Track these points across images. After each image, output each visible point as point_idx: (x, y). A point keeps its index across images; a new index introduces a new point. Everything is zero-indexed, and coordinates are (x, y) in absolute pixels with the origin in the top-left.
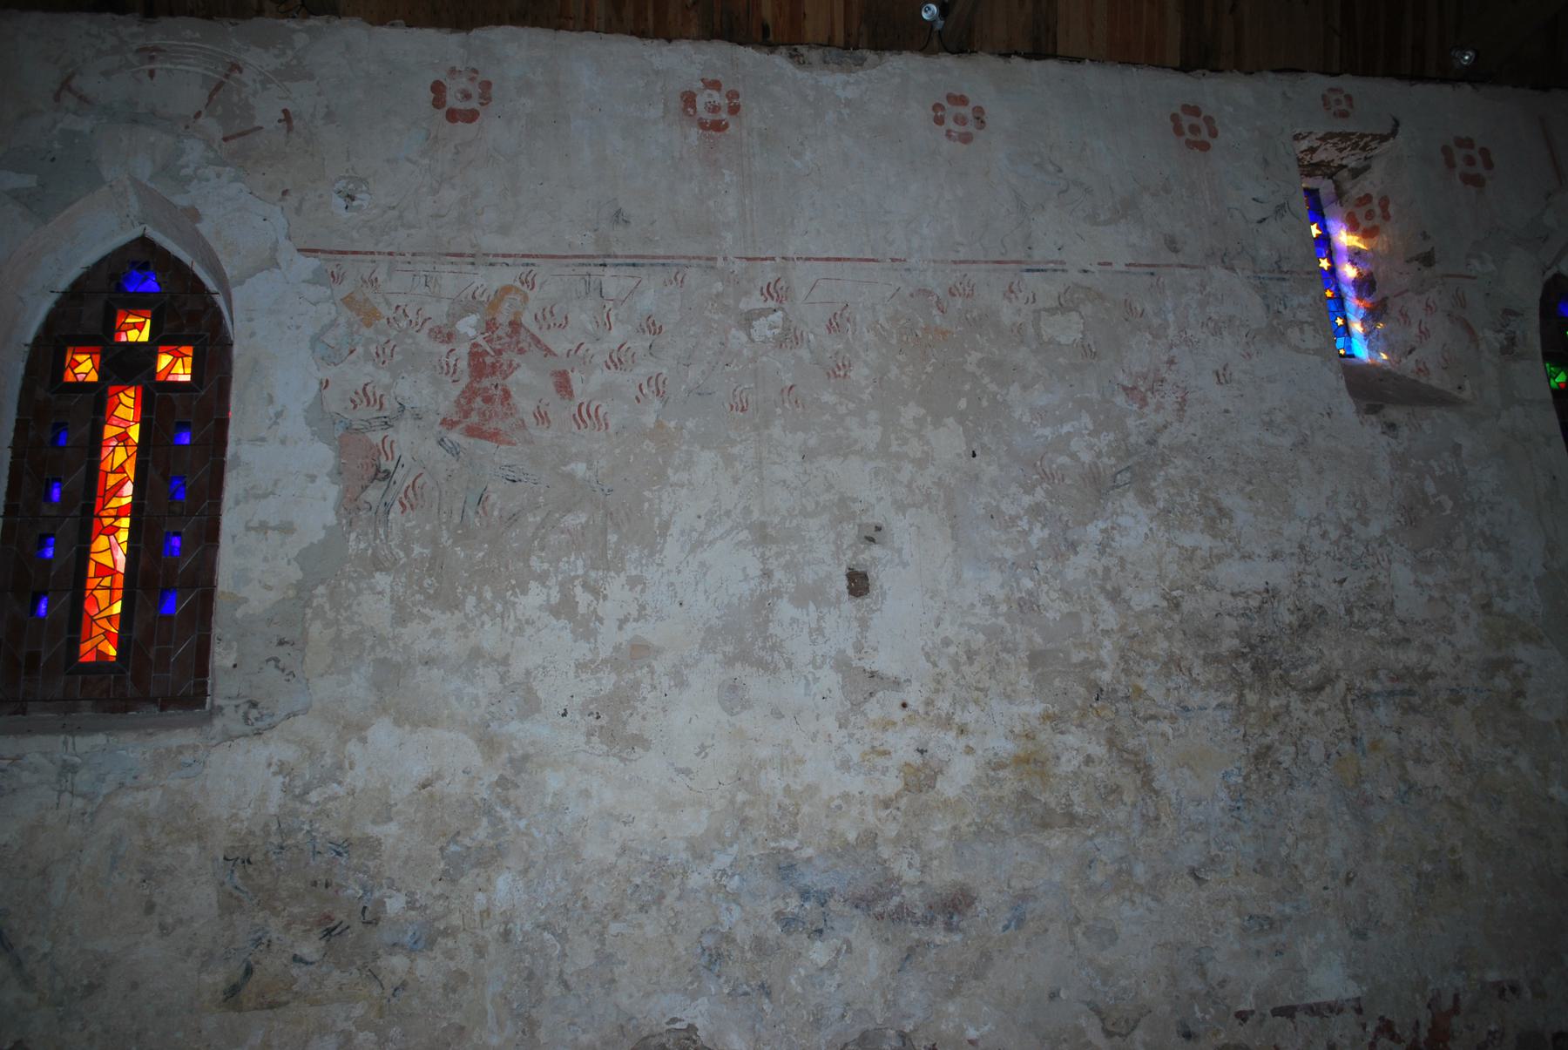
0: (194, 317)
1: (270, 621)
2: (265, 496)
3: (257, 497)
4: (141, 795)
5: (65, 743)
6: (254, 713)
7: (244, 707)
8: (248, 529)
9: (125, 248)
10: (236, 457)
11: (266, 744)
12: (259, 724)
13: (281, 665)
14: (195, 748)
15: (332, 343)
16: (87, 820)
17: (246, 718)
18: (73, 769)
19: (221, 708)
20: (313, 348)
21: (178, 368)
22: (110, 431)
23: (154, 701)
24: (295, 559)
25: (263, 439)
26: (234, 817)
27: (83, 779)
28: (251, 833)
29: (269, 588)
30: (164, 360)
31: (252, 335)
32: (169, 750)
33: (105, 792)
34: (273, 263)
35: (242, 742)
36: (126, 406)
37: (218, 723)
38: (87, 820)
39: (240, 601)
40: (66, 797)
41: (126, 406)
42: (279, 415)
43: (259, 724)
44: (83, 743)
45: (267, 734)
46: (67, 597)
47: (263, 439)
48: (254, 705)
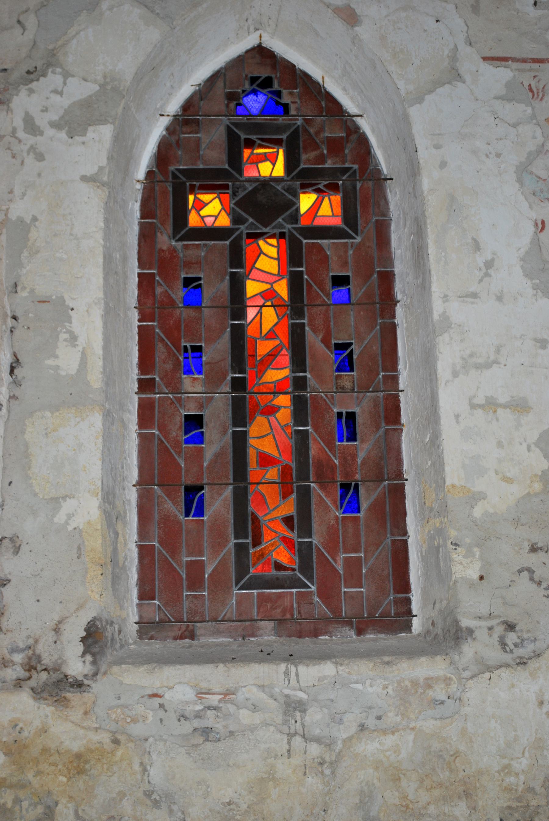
0: (333, 150)
1: (517, 522)
2: (488, 365)
3: (478, 367)
4: (390, 740)
5: (287, 674)
6: (512, 638)
7: (499, 630)
8: (473, 406)
9: (239, 62)
10: (445, 317)
11: (533, 675)
12: (520, 652)
13: (536, 577)
14: (447, 681)
15: (543, 174)
16: (327, 772)
17: (503, 644)
18: (300, 706)
19: (470, 631)
20: (520, 181)
21: (325, 209)
22: (252, 288)
23: (348, 622)
24: (537, 444)
25: (474, 295)
26: (507, 769)
27: (315, 717)
28: (530, 790)
29: (508, 480)
30: (306, 201)
31: (443, 165)
32: (415, 683)
33: (345, 736)
34: (454, 75)
35: (504, 673)
36: (268, 256)
37: (469, 650)
38: (327, 772)
39: (476, 498)
40: (298, 741)
41: (268, 256)
42: (489, 264)
43: (520, 652)
44: (310, 673)
45: (533, 665)
46: (228, 492)
47: (474, 295)
48: (511, 627)
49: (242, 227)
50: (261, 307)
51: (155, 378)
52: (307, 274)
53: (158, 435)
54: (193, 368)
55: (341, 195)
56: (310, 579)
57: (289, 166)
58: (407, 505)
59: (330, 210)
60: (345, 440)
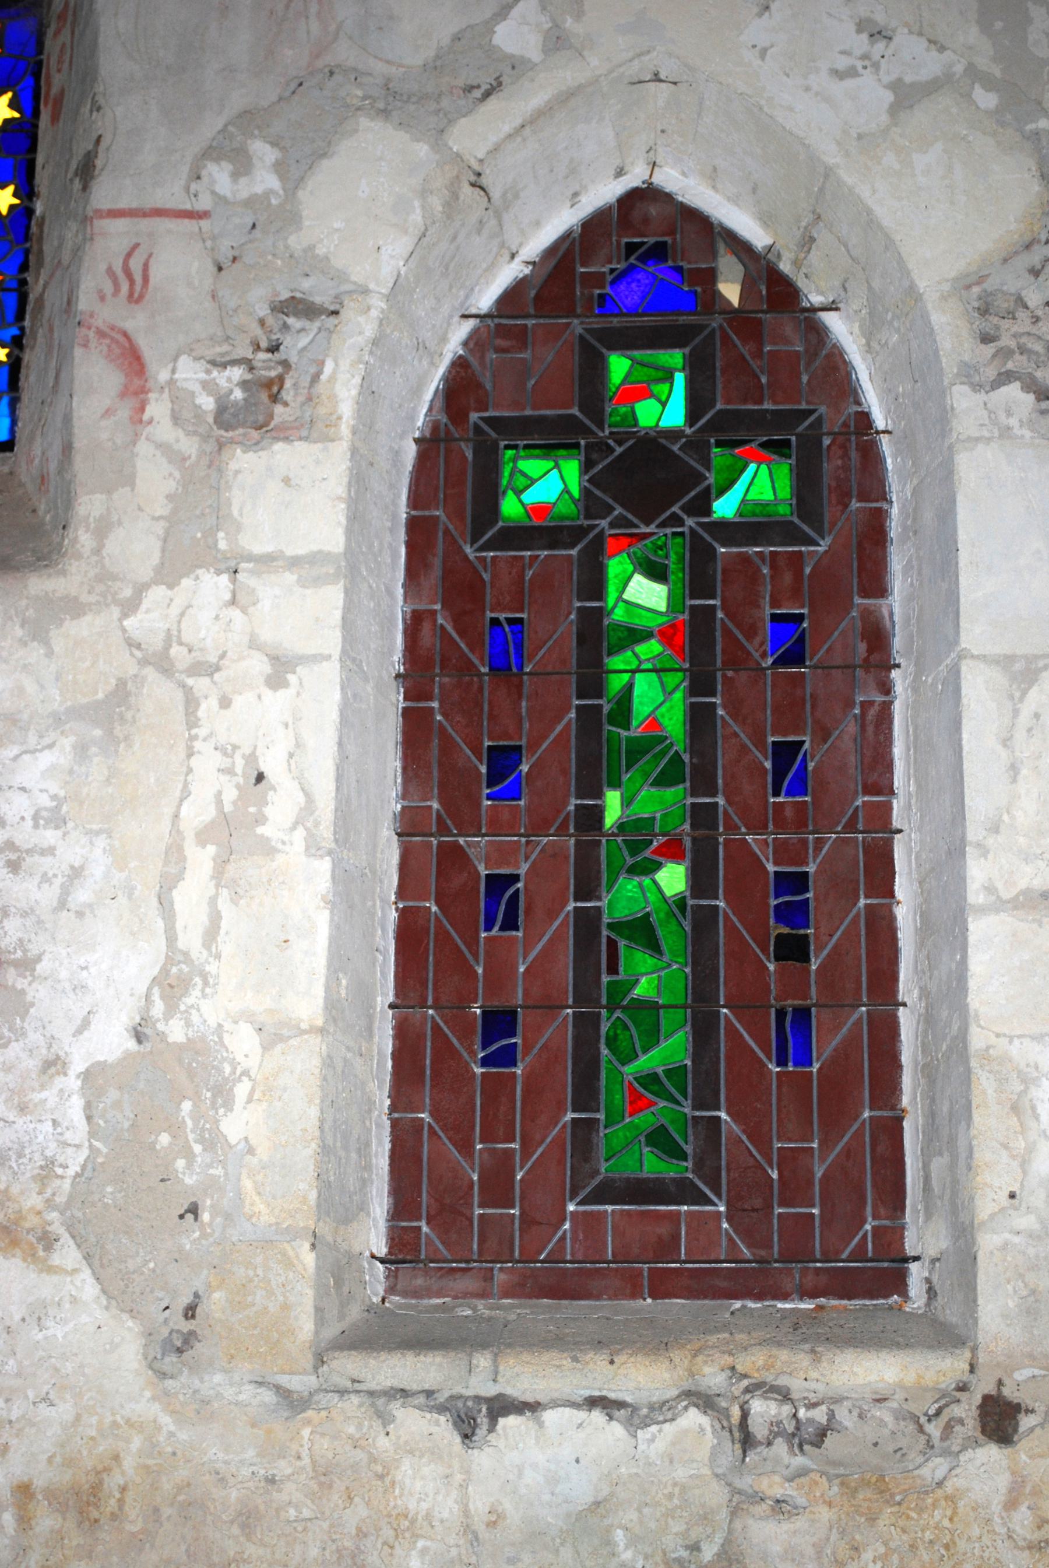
49: (604, 523)
50: (633, 672)
51: (419, 1228)
52: (729, 1221)
53: (433, 1017)
54: (507, 629)
55: (793, 461)
56: (719, 1195)
57: (695, 407)
58: (896, 856)
59: (771, 492)
60: (783, 793)
